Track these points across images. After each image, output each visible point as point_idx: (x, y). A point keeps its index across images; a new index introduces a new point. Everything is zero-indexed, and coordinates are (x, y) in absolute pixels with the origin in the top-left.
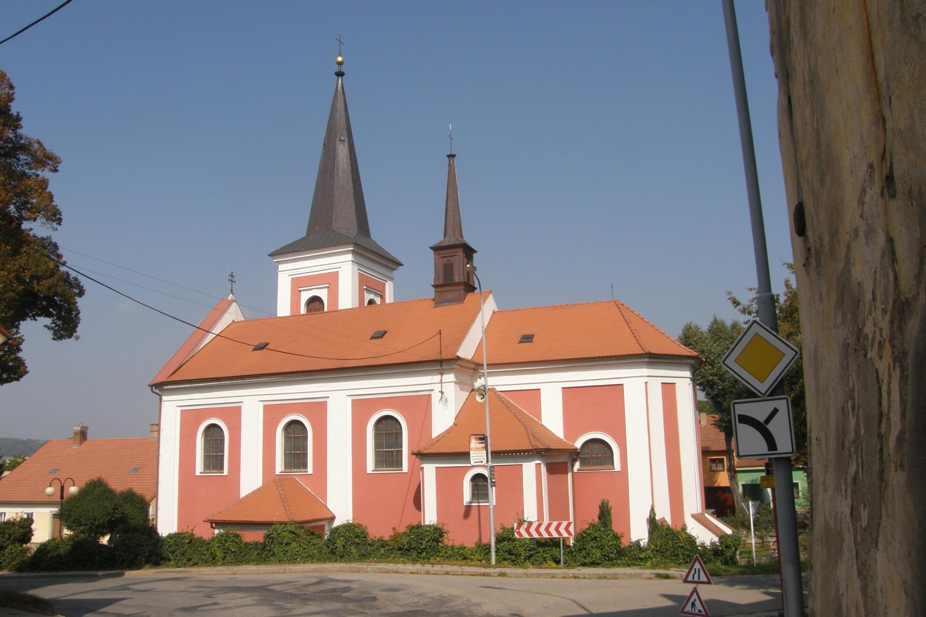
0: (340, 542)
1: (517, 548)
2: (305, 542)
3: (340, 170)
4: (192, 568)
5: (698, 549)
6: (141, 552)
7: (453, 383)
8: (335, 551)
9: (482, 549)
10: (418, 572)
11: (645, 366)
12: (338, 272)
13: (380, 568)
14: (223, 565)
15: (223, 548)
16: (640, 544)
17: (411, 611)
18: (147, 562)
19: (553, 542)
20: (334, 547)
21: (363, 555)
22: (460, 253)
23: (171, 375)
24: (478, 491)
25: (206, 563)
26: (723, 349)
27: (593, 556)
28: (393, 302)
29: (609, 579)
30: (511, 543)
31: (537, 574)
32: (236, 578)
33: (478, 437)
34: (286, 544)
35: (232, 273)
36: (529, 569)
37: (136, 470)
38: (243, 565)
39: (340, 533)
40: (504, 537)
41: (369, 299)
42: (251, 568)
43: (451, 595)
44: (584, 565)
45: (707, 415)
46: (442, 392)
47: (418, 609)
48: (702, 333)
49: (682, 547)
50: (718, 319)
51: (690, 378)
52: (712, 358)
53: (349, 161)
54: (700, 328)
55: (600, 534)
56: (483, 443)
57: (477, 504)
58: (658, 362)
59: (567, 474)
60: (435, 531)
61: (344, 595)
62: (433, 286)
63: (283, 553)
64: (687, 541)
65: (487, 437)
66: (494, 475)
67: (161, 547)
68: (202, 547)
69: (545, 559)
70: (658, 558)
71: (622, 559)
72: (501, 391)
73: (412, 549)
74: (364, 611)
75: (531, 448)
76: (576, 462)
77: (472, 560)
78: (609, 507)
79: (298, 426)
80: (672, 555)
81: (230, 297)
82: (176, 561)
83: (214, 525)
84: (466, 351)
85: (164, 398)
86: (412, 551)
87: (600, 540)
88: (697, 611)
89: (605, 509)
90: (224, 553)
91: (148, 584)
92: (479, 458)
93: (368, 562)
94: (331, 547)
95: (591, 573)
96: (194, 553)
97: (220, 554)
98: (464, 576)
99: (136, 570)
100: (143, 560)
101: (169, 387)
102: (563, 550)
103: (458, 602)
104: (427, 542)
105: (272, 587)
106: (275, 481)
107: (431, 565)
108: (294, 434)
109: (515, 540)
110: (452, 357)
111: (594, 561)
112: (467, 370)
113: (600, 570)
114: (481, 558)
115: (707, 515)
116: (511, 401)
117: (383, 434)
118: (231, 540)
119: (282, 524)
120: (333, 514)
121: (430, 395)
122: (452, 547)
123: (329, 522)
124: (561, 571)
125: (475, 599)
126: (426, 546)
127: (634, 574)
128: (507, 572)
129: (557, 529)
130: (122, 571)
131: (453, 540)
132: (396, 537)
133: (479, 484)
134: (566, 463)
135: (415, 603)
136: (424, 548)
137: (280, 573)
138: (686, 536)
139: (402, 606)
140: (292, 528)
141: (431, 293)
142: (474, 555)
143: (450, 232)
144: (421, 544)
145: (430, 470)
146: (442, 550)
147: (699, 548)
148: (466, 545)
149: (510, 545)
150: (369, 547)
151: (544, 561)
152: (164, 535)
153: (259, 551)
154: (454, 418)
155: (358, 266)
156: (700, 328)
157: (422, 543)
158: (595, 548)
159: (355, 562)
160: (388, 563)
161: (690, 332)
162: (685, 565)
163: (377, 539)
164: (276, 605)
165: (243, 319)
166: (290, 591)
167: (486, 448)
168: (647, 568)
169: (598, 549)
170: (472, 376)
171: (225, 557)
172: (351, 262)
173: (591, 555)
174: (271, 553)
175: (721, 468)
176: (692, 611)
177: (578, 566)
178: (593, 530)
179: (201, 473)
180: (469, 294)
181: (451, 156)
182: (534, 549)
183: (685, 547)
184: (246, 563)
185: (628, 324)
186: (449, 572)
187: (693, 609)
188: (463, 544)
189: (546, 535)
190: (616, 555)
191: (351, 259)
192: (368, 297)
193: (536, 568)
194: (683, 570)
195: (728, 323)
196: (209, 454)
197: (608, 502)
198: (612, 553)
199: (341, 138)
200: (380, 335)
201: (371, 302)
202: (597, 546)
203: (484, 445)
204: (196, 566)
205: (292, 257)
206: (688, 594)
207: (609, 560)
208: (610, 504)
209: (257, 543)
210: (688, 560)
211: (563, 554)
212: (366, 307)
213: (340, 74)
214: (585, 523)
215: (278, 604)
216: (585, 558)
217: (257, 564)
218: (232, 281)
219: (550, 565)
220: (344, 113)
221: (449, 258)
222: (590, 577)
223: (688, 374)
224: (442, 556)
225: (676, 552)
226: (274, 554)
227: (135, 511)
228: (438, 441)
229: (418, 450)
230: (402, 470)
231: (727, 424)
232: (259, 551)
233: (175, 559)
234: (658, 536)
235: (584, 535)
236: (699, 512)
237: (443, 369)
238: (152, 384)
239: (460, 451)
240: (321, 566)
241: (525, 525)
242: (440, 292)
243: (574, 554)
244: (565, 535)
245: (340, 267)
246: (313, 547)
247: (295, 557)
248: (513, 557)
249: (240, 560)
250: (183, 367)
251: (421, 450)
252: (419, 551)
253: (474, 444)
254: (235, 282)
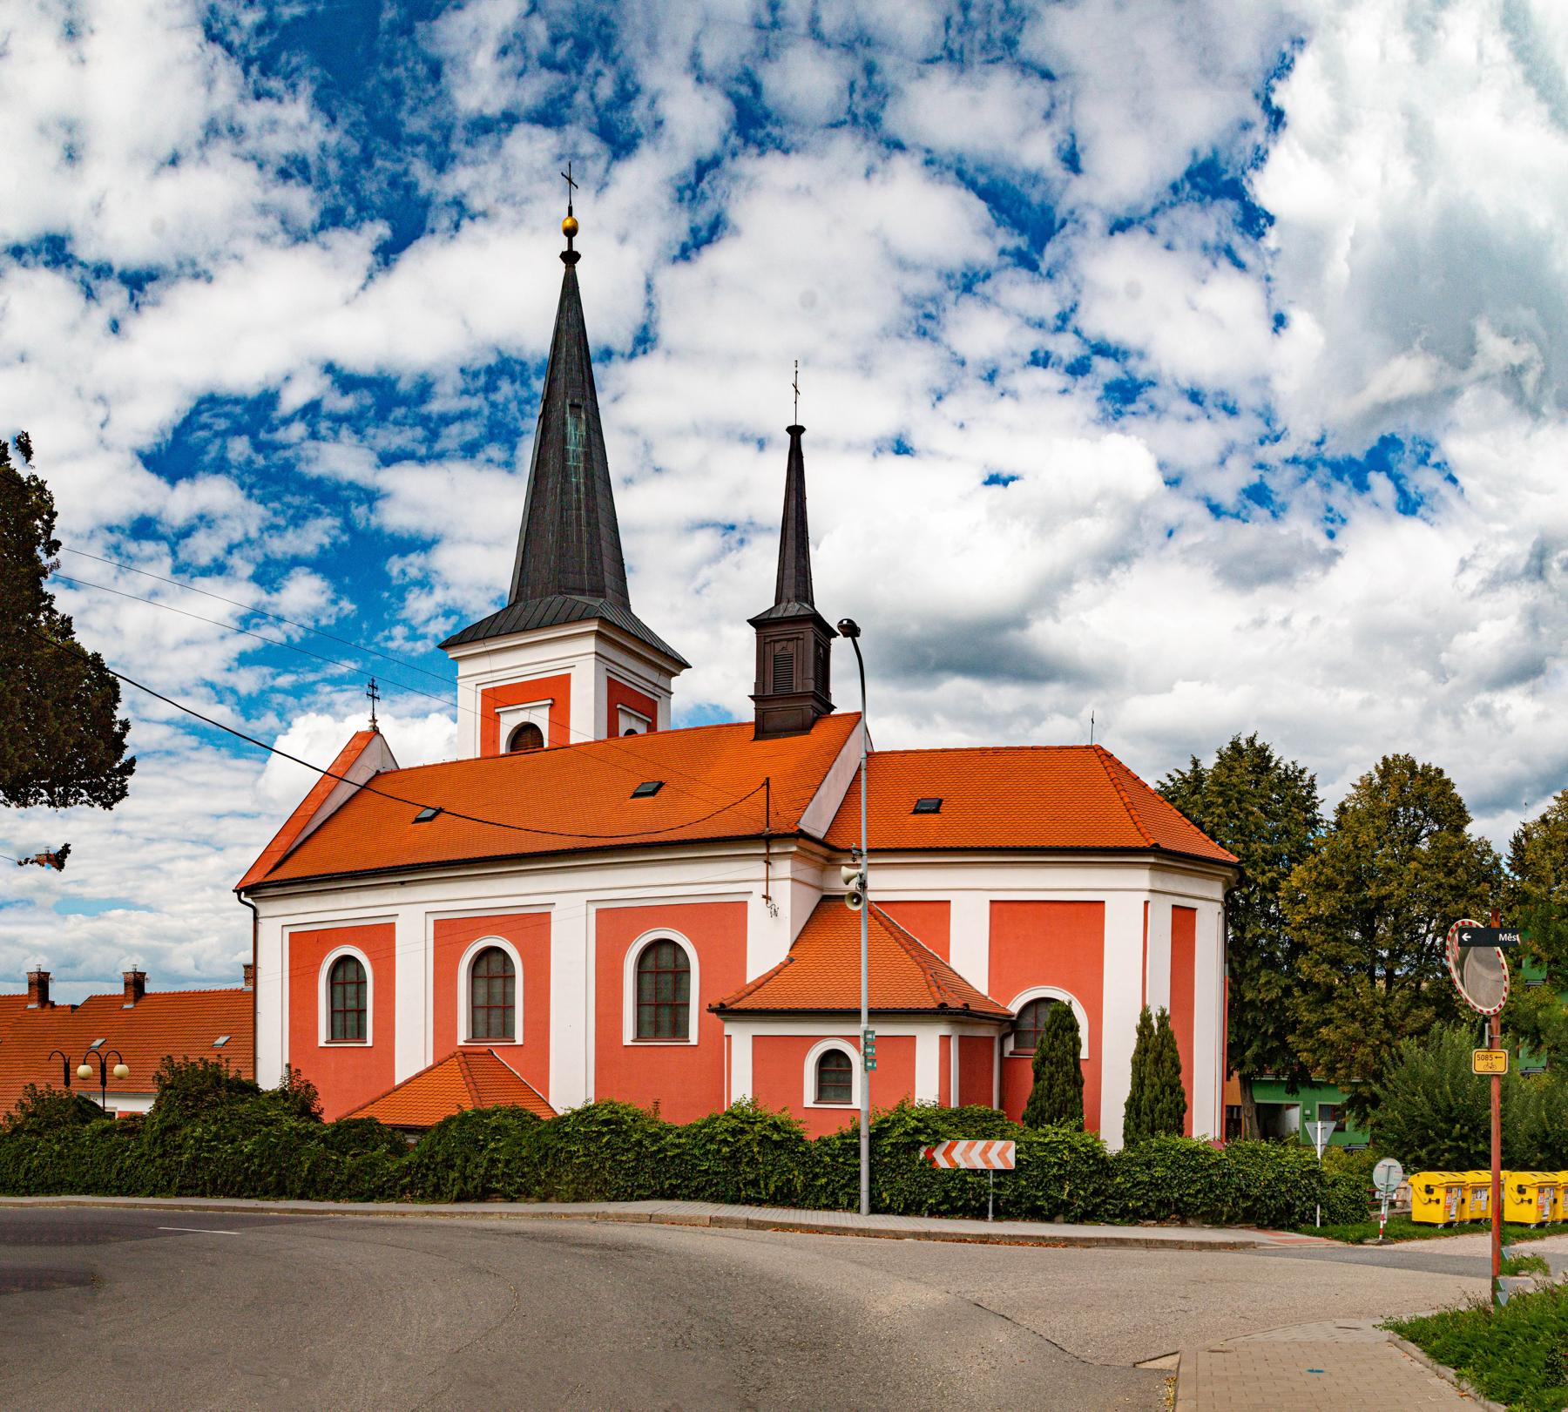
84: (817, 820)
145: (741, 1039)
201: (630, 732)
221: (784, 643)
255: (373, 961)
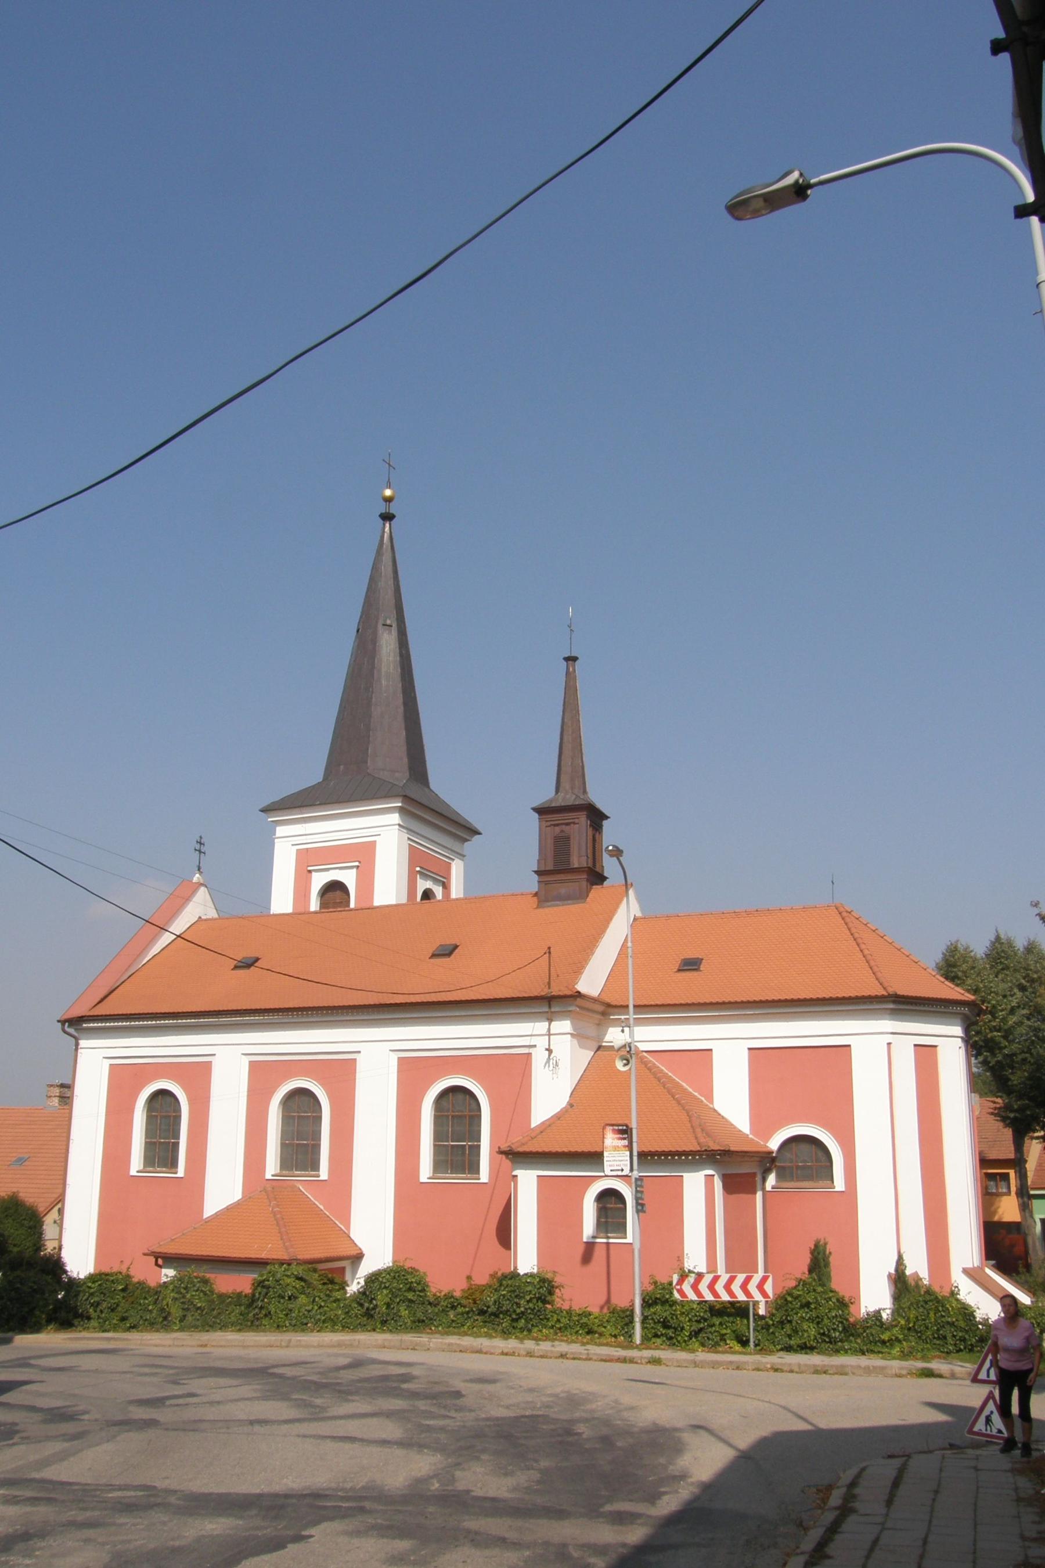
0: (382, 1298)
1: (677, 1318)
2: (322, 1295)
3: (383, 674)
4: (128, 1333)
5: (978, 1328)
6: (41, 1303)
7: (569, 1036)
8: (373, 1312)
9: (619, 1317)
10: (514, 1352)
11: (888, 1016)
12: (375, 842)
13: (450, 1344)
14: (181, 1329)
15: (181, 1301)
16: (881, 1317)
17: (526, 1417)
18: (49, 1321)
19: (734, 1308)
20: (372, 1306)
21: (419, 1321)
22: (583, 819)
23: (96, 1005)
24: (606, 1217)
25: (152, 1325)
26: (1011, 987)
27: (803, 1335)
28: (462, 896)
29: (833, 1374)
30: (667, 1307)
31: (712, 1361)
32: (207, 1353)
33: (616, 1128)
34: (290, 1298)
35: (201, 837)
36: (697, 1353)
37: (20, 1161)
38: (215, 1331)
39: (382, 1282)
40: (656, 1298)
41: (423, 890)
42: (231, 1336)
43: (584, 1392)
44: (788, 1349)
45: (980, 1097)
46: (549, 1051)
47: (535, 1413)
48: (975, 960)
49: (952, 1324)
50: (1002, 937)
51: (962, 1038)
52: (994, 1002)
53: (398, 658)
54: (972, 951)
55: (816, 1298)
56: (624, 1139)
57: (604, 1240)
58: (915, 1010)
59: (755, 1193)
60: (541, 1284)
61: (405, 1386)
62: (536, 872)
63: (284, 1313)
64: (960, 1314)
65: (631, 1129)
66: (642, 1192)
67: (77, 1296)
68: (145, 1298)
69: (723, 1338)
70: (911, 1342)
71: (851, 1342)
72: (646, 1052)
73: (501, 1312)
74: (448, 1414)
75: (699, 1149)
76: (771, 1174)
77: (601, 1335)
78: (827, 1252)
79: (305, 1099)
80: (934, 1338)
81: (197, 878)
82: (101, 1321)
83: (160, 1261)
85: (83, 1043)
86: (501, 1316)
87: (815, 1308)
88: (994, 1432)
89: (820, 1256)
90: (183, 1309)
91: (60, 1358)
92: (618, 1163)
93: (428, 1333)
94: (366, 1305)
95: (802, 1363)
96: (132, 1308)
97: (176, 1311)
98: (591, 1362)
99: (32, 1333)
100: (44, 1316)
101: (92, 1025)
102: (754, 1322)
103: (599, 1403)
104: (528, 1302)
105: (276, 1370)
106: (265, 1190)
107: (534, 1342)
108: (298, 1112)
109: (675, 1303)
110: (569, 993)
111: (805, 1342)
112: (590, 1014)
113: (815, 1359)
114: (616, 1332)
115: (988, 1271)
116: (663, 1068)
117: (448, 1116)
118: (195, 1289)
119: (283, 1264)
120: (360, 1249)
121: (530, 1054)
122: (569, 1312)
123: (353, 1262)
124: (752, 1359)
125: (627, 1400)
126: (526, 1309)
127: (873, 1366)
128: (661, 1357)
129: (744, 1287)
130: (10, 1334)
131: (571, 1300)
132: (473, 1292)
133: (609, 1206)
134: (754, 1175)
135: (528, 1402)
136: (523, 1313)
137: (281, 1347)
138: (959, 1306)
139: (507, 1407)
140: (299, 1270)
141: (532, 883)
142: (605, 1327)
143: (566, 784)
144: (518, 1305)
146: (552, 1316)
147: (980, 1326)
148: (592, 1310)
149: (665, 1311)
150: (429, 1307)
151: (721, 1340)
152: (82, 1276)
153: (243, 1308)
154: (569, 1095)
155: (407, 833)
156: (972, 951)
157: (519, 1304)
158: (807, 1320)
159: (406, 1333)
160: (463, 1336)
161: (956, 957)
162: (957, 1355)
163: (443, 1294)
164: (296, 1400)
165: (216, 916)
166: (309, 1378)
167: (630, 1147)
168: (894, 1358)
169: (812, 1322)
170: (598, 1025)
171: (185, 1316)
172: (397, 827)
173: (800, 1334)
174: (263, 1312)
175: (1005, 1190)
176: (986, 1430)
177: (778, 1351)
178: (803, 1290)
179: (138, 1172)
180: (594, 887)
181: (571, 659)
182: (705, 1320)
183: (956, 1324)
184: (220, 1329)
185: (858, 945)
186: (566, 1354)
187: (989, 1428)
188: (585, 1308)
189: (725, 1297)
190: (843, 1335)
191: (397, 822)
192: (423, 885)
193: (708, 1352)
194: (935, 1365)
195: (1020, 944)
196: (153, 1140)
197: (826, 1244)
198: (834, 1330)
199: (385, 620)
200: (447, 951)
201: (427, 895)
202: (810, 1318)
203: (626, 1142)
204: (134, 1330)
205: (300, 814)
206: (977, 1403)
207: (830, 1342)
208: (828, 1247)
209: (239, 1295)
210: (962, 1347)
211: (754, 1330)
212: (419, 903)
213: (388, 517)
214: (791, 1279)
215: (302, 1399)
216: (790, 1337)
217: (240, 1330)
218: (200, 851)
219: (731, 1348)
220: (392, 580)
222: (801, 1370)
223: (958, 1030)
224: (552, 1327)
225: (941, 1332)
226: (268, 1314)
227: (20, 1232)
228: (542, 1132)
229: (509, 1146)
230: (479, 1179)
231: (1017, 1115)
232: (243, 1308)
233: (99, 1317)
234: (912, 1304)
235: (789, 1299)
236: (976, 1265)
237: (552, 1012)
238: (66, 1017)
239: (579, 1150)
240: (352, 1338)
241: (691, 1279)
242: (547, 883)
243: (771, 1330)
244: (757, 1296)
245: (379, 835)
246: (335, 1305)
247: (305, 1321)
248: (670, 1332)
249: (211, 1323)
250: (115, 992)
251: (513, 1146)
252: (514, 1316)
253: (611, 1140)
254: (204, 853)
255: (191, 1102)
